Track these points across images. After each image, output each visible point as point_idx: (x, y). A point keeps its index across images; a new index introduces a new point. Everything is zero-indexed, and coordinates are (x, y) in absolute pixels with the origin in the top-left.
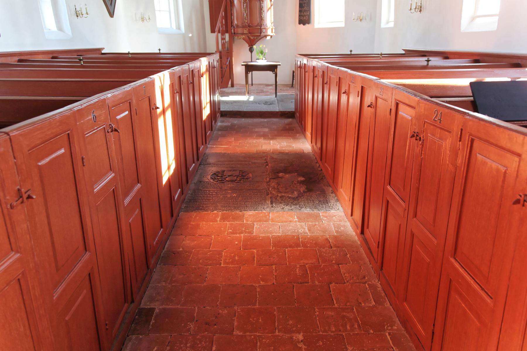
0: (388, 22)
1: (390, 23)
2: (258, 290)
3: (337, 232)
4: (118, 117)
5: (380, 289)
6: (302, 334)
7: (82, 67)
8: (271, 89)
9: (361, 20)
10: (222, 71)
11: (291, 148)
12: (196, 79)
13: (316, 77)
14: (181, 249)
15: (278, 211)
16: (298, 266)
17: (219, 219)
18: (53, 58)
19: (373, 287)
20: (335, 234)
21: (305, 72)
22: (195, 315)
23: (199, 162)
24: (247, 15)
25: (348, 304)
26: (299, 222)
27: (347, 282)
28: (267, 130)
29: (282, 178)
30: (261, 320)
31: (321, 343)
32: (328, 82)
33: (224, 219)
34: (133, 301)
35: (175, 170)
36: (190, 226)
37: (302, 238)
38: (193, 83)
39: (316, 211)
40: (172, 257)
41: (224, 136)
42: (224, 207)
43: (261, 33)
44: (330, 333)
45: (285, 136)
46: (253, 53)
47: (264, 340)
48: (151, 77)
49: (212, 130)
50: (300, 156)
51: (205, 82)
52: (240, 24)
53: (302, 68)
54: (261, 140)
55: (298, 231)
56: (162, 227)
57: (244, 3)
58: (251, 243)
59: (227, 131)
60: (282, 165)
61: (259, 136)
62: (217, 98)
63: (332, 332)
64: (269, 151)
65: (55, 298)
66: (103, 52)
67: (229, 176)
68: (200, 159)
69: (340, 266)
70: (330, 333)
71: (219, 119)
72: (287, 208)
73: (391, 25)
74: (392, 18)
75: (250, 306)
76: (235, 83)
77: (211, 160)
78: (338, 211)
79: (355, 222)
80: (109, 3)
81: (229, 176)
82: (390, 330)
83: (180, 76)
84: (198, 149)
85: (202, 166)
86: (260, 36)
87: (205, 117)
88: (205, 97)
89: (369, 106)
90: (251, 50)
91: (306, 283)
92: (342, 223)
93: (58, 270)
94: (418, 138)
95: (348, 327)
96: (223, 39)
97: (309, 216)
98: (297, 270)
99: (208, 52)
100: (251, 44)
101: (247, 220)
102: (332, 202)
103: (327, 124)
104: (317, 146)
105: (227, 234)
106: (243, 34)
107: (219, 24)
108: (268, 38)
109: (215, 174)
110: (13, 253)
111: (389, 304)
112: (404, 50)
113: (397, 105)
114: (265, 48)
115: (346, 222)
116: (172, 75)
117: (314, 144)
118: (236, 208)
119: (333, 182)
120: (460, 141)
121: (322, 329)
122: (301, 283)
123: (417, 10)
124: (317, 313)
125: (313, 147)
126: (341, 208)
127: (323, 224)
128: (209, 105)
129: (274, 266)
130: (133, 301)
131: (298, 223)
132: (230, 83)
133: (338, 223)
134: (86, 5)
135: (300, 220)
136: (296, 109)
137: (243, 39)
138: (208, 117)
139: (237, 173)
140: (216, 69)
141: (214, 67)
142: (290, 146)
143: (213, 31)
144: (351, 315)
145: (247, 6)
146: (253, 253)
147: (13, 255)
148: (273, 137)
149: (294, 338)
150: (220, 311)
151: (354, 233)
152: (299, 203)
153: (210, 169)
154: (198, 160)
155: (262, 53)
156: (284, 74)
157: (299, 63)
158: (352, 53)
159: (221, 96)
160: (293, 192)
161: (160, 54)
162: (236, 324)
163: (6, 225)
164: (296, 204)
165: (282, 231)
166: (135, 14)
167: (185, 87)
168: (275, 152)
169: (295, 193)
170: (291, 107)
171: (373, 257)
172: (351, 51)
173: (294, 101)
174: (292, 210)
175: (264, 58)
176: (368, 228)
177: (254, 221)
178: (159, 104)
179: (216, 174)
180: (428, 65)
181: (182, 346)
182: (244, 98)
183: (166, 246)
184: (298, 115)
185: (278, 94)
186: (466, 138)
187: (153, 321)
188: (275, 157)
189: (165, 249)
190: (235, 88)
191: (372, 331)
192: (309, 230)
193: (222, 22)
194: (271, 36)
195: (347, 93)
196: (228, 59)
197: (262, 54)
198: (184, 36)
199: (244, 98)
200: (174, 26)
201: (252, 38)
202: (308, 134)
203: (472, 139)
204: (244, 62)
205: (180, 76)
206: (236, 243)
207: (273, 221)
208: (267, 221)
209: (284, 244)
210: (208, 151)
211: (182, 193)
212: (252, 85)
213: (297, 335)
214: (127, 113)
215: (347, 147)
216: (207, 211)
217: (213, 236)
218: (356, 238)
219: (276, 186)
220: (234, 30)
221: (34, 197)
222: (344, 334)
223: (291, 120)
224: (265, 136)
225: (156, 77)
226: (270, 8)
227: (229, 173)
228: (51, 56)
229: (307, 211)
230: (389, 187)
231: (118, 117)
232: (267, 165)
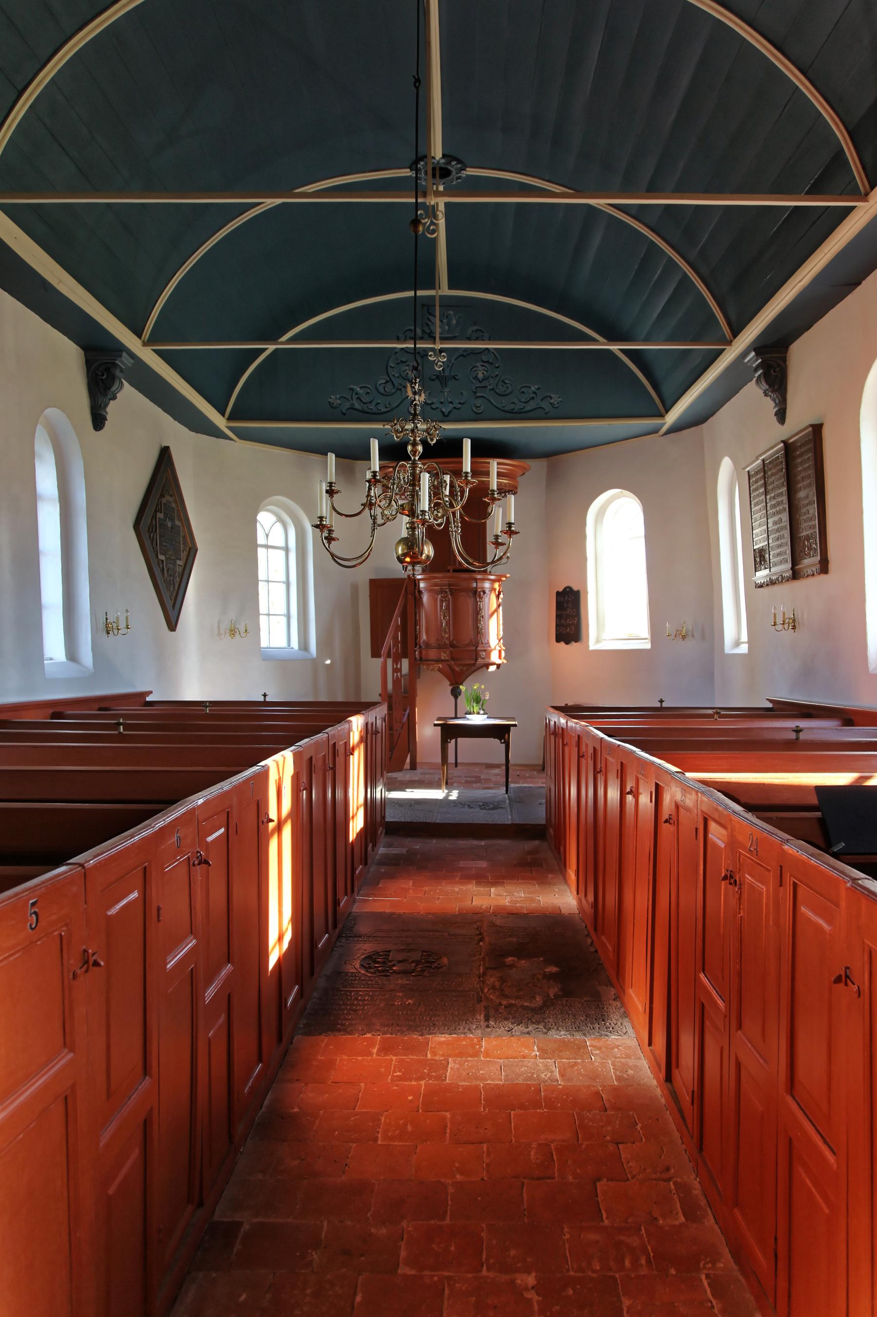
0: (737, 643)
1: (742, 645)
2: (451, 1190)
3: (619, 1078)
4: (210, 839)
5: (697, 1190)
6: (534, 1274)
7: (121, 738)
8: (496, 775)
9: (684, 637)
10: (391, 735)
11: (534, 905)
12: (340, 760)
13: (583, 756)
14: (296, 1110)
15: (499, 1036)
16: (534, 1145)
17: (375, 1051)
18: (55, 716)
19: (684, 1188)
20: (616, 1083)
21: (564, 745)
22: (323, 1236)
23: (337, 931)
24: (448, 624)
25: (630, 1220)
26: (541, 1057)
27: (633, 1177)
28: (483, 864)
29: (511, 966)
30: (453, 1248)
31: (571, 1292)
32: (603, 769)
33: (386, 1049)
34: (201, 1204)
35: (290, 943)
36: (314, 1063)
37: (545, 1091)
38: (333, 769)
39: (578, 1036)
40: (280, 1125)
41: (391, 876)
42: (388, 1026)
43: (476, 660)
44: (590, 1273)
45: (523, 878)
46: (460, 698)
47: (457, 1285)
48: (262, 763)
49: (366, 864)
50: (555, 921)
51: (357, 763)
52: (433, 641)
53: (558, 733)
54: (470, 886)
55: (538, 1076)
56: (260, 1060)
57: (442, 601)
58: (440, 1098)
59: (399, 866)
60: (514, 940)
61: (467, 877)
62: (379, 792)
63: (594, 1271)
64: (487, 910)
65: (102, 1144)
66: (148, 699)
67: (400, 962)
68: (340, 926)
69: (620, 1146)
70: (590, 1273)
71: (383, 840)
72: (518, 1029)
73: (744, 649)
74: (744, 637)
75: (432, 1222)
76: (418, 760)
77: (363, 928)
78: (626, 1037)
79: (655, 1058)
80: (169, 604)
81: (400, 962)
82: (709, 1269)
83: (311, 758)
84: (336, 903)
85: (343, 940)
86: (474, 664)
87: (352, 836)
88: (357, 793)
89: (666, 821)
90: (456, 693)
91: (549, 1178)
92: (631, 1062)
93: (109, 1096)
94: (732, 881)
95: (627, 1263)
96: (396, 670)
97: (564, 1045)
98: (532, 1153)
99: (364, 699)
100: (456, 681)
101: (434, 1053)
102: (614, 1018)
103: (603, 851)
104: (587, 901)
105: (392, 1079)
106: (439, 661)
107: (388, 641)
108: (492, 668)
109: (369, 957)
110: (66, 1051)
111: (713, 1221)
112: (771, 701)
113: (706, 821)
114: (484, 691)
115: (640, 1058)
116: (297, 757)
117: (582, 895)
118: (412, 1028)
119: (615, 976)
120: (781, 886)
121: (575, 1266)
122: (538, 1179)
123: (786, 626)
124: (568, 1236)
125: (580, 901)
126: (631, 1031)
127: (592, 1063)
128: (361, 811)
129: (485, 1146)
130: (201, 1204)
131: (540, 1061)
132: (408, 760)
133: (623, 1060)
134: (127, 611)
135: (544, 1053)
136: (548, 819)
137: (439, 670)
138: (359, 835)
139: (417, 956)
140: (379, 735)
141: (377, 732)
142: (532, 900)
143: (375, 653)
144: (634, 1241)
145: (448, 606)
146: (444, 1118)
147: (65, 1055)
148: (497, 881)
149: (519, 1281)
150: (373, 1230)
151: (655, 1082)
152: (544, 1019)
153: (359, 946)
154: (335, 926)
155: (478, 700)
156: (525, 745)
157: (552, 723)
158: (664, 705)
159: (389, 790)
160: (535, 998)
161: (265, 703)
162: (403, 1254)
163: (64, 1005)
164: (538, 1023)
165: (506, 1076)
166: (219, 623)
167: (321, 774)
168: (500, 912)
169: (538, 998)
170: (539, 815)
171: (686, 1126)
172: (661, 701)
173: (544, 801)
174: (528, 1033)
175: (482, 712)
176: (677, 1067)
177: (449, 1056)
178: (273, 814)
179: (371, 958)
180: (797, 739)
181: (296, 1292)
182: (438, 794)
183: (266, 1102)
184: (551, 831)
185: (512, 785)
186: (788, 880)
187: (238, 1247)
188: (498, 922)
189: (263, 1109)
190: (419, 770)
191: (673, 1271)
192: (562, 1075)
193: (395, 638)
194: (498, 666)
195: (636, 794)
196: (405, 710)
197: (477, 703)
198: (315, 663)
199: (438, 794)
200: (295, 644)
201: (457, 669)
202: (572, 874)
203: (794, 882)
204: (438, 719)
205: (311, 758)
206: (410, 1098)
207: (487, 1054)
208: (476, 1054)
209: (507, 1100)
210: (355, 909)
211: (301, 994)
212: (456, 764)
213: (524, 1276)
214: (222, 830)
215: (638, 900)
216: (351, 1033)
217: (362, 1085)
218: (659, 1092)
219: (497, 984)
220: (420, 653)
221: (102, 964)
222: (617, 1276)
223: (532, 841)
224: (480, 878)
225: (269, 762)
226: (496, 610)
227: (401, 956)
228: (51, 711)
229: (560, 1035)
230: (702, 976)
231: (210, 839)
232: (481, 940)
